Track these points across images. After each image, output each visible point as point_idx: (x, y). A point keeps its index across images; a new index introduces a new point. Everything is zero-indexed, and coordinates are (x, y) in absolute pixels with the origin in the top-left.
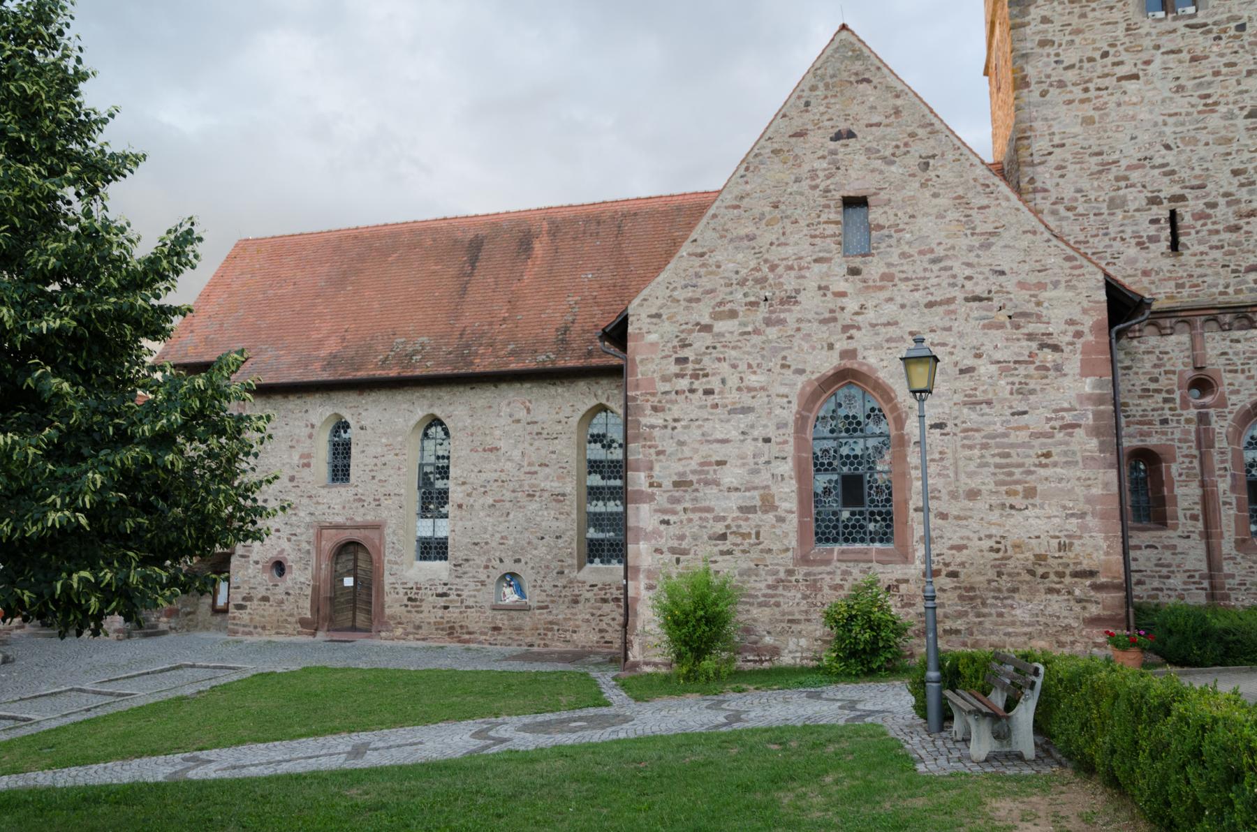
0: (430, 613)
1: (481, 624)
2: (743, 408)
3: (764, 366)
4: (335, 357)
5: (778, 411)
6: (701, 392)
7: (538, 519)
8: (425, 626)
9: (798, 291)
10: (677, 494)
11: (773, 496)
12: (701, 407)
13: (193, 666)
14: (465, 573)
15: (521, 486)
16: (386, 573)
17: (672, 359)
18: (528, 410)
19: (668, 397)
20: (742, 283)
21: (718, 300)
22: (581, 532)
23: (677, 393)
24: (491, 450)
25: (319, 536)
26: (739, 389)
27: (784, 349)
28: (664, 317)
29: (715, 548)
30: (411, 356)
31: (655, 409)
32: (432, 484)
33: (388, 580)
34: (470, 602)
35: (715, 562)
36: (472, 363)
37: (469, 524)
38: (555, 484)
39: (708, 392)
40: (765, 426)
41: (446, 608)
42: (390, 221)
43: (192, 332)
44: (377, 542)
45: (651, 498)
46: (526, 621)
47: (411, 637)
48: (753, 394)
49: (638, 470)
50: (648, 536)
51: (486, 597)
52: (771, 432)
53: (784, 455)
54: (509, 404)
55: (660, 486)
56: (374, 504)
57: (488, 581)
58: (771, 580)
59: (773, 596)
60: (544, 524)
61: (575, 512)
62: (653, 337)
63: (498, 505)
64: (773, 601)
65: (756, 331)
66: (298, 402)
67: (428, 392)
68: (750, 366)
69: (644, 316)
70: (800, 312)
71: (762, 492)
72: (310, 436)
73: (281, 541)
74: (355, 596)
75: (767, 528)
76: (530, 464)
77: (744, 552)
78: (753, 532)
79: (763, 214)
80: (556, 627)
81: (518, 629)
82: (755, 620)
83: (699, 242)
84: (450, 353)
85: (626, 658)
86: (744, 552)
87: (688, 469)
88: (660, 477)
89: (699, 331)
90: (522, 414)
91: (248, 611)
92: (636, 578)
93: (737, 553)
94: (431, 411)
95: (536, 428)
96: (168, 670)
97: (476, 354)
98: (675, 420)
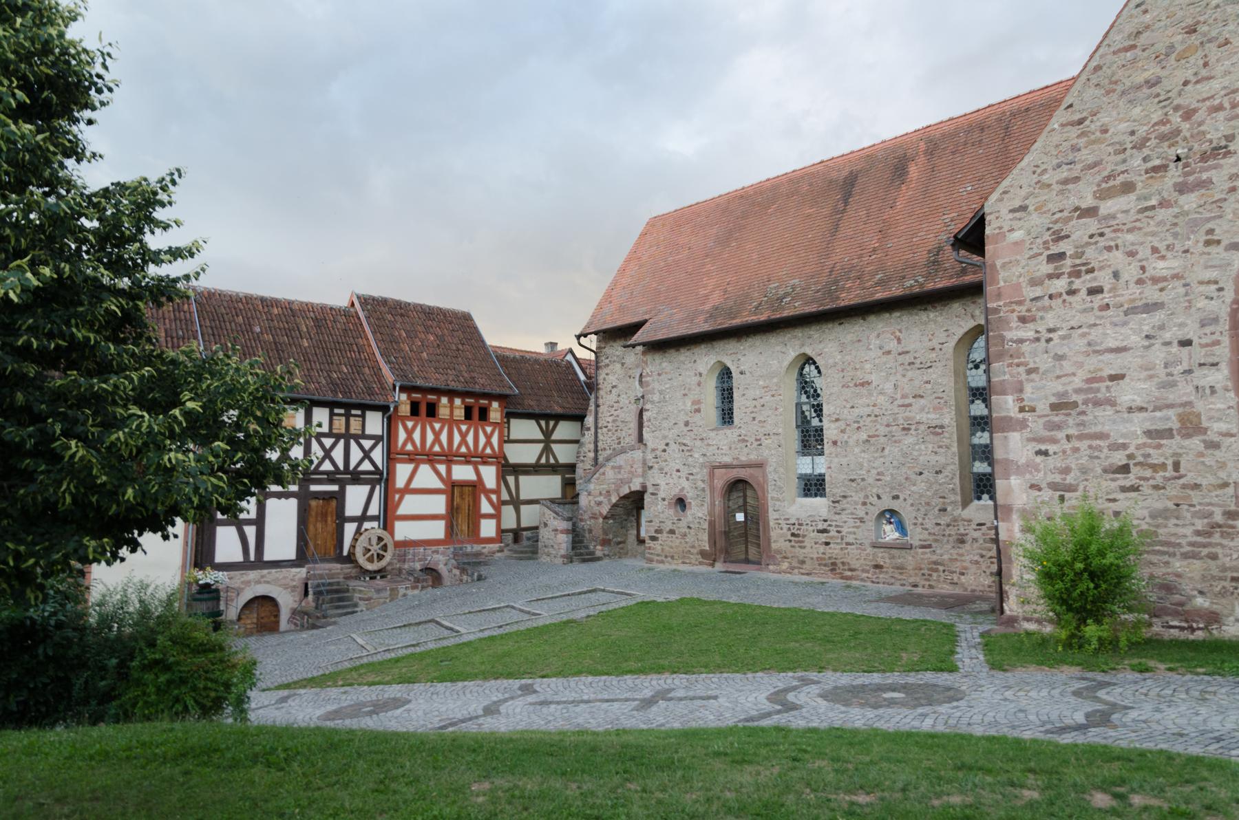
0: (812, 548)
1: (862, 561)
2: (1147, 305)
3: (1178, 247)
4: (717, 309)
5: (1201, 303)
6: (1084, 292)
7: (915, 453)
8: (808, 561)
9: (1230, 138)
10: (1056, 419)
11: (1199, 415)
12: (1085, 311)
13: (603, 591)
14: (843, 510)
15: (894, 420)
16: (770, 509)
17: (1044, 257)
18: (899, 340)
19: (1039, 304)
20: (1139, 146)
21: (1106, 173)
22: (964, 467)
23: (1051, 297)
24: (862, 385)
25: (712, 475)
26: (1140, 282)
27: (1208, 220)
28: (1031, 208)
29: (1111, 484)
30: (781, 299)
31: (1023, 320)
32: (809, 422)
33: (772, 516)
34: (850, 539)
35: (1114, 500)
36: (838, 298)
37: (844, 461)
38: (932, 416)
39: (1095, 291)
40: (1182, 325)
41: (827, 544)
42: (771, 176)
43: (611, 302)
44: (761, 479)
45: (1023, 425)
46: (909, 559)
47: (796, 571)
48: (1161, 285)
49: (1004, 393)
50: (1020, 470)
51: (866, 533)
52: (1191, 332)
53: (1215, 360)
54: (878, 336)
55: (1033, 410)
56: (756, 443)
57: (866, 518)
58: (1200, 524)
59: (1204, 546)
60: (921, 458)
61: (956, 444)
62: (1017, 235)
63: (872, 440)
64: (1205, 551)
65: (1164, 204)
66: (688, 353)
67: (798, 332)
68: (1155, 250)
69: (1004, 212)
70: (1233, 165)
71: (1180, 410)
72: (699, 384)
73: (681, 480)
74: (746, 530)
75: (1191, 457)
76: (904, 397)
77: (1156, 487)
78: (1170, 462)
79: (1172, 47)
80: (941, 568)
81: (900, 568)
82: (1179, 576)
83: (1076, 107)
84: (818, 291)
85: (1002, 611)
86: (1156, 487)
87: (1070, 388)
88: (1032, 400)
89: (1079, 217)
90: (892, 345)
91: (660, 542)
92: (1007, 518)
93: (1146, 490)
94: (802, 351)
95: (908, 358)
96: (585, 593)
97: (843, 289)
98: (1050, 331)
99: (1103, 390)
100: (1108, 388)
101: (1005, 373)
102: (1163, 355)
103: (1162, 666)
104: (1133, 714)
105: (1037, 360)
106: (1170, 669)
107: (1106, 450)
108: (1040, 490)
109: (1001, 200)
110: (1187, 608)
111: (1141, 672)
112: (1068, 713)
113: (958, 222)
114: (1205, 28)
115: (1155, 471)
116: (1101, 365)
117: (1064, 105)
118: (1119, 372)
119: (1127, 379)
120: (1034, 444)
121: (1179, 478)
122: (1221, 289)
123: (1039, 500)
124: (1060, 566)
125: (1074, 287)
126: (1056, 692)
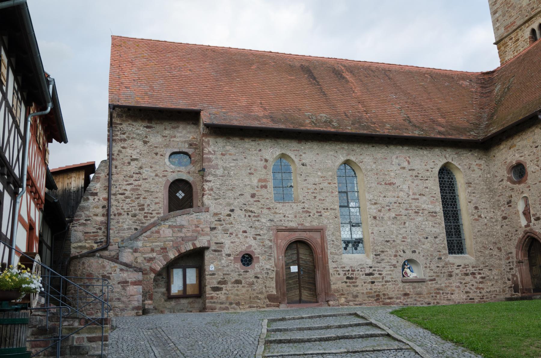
80: (441, 292)
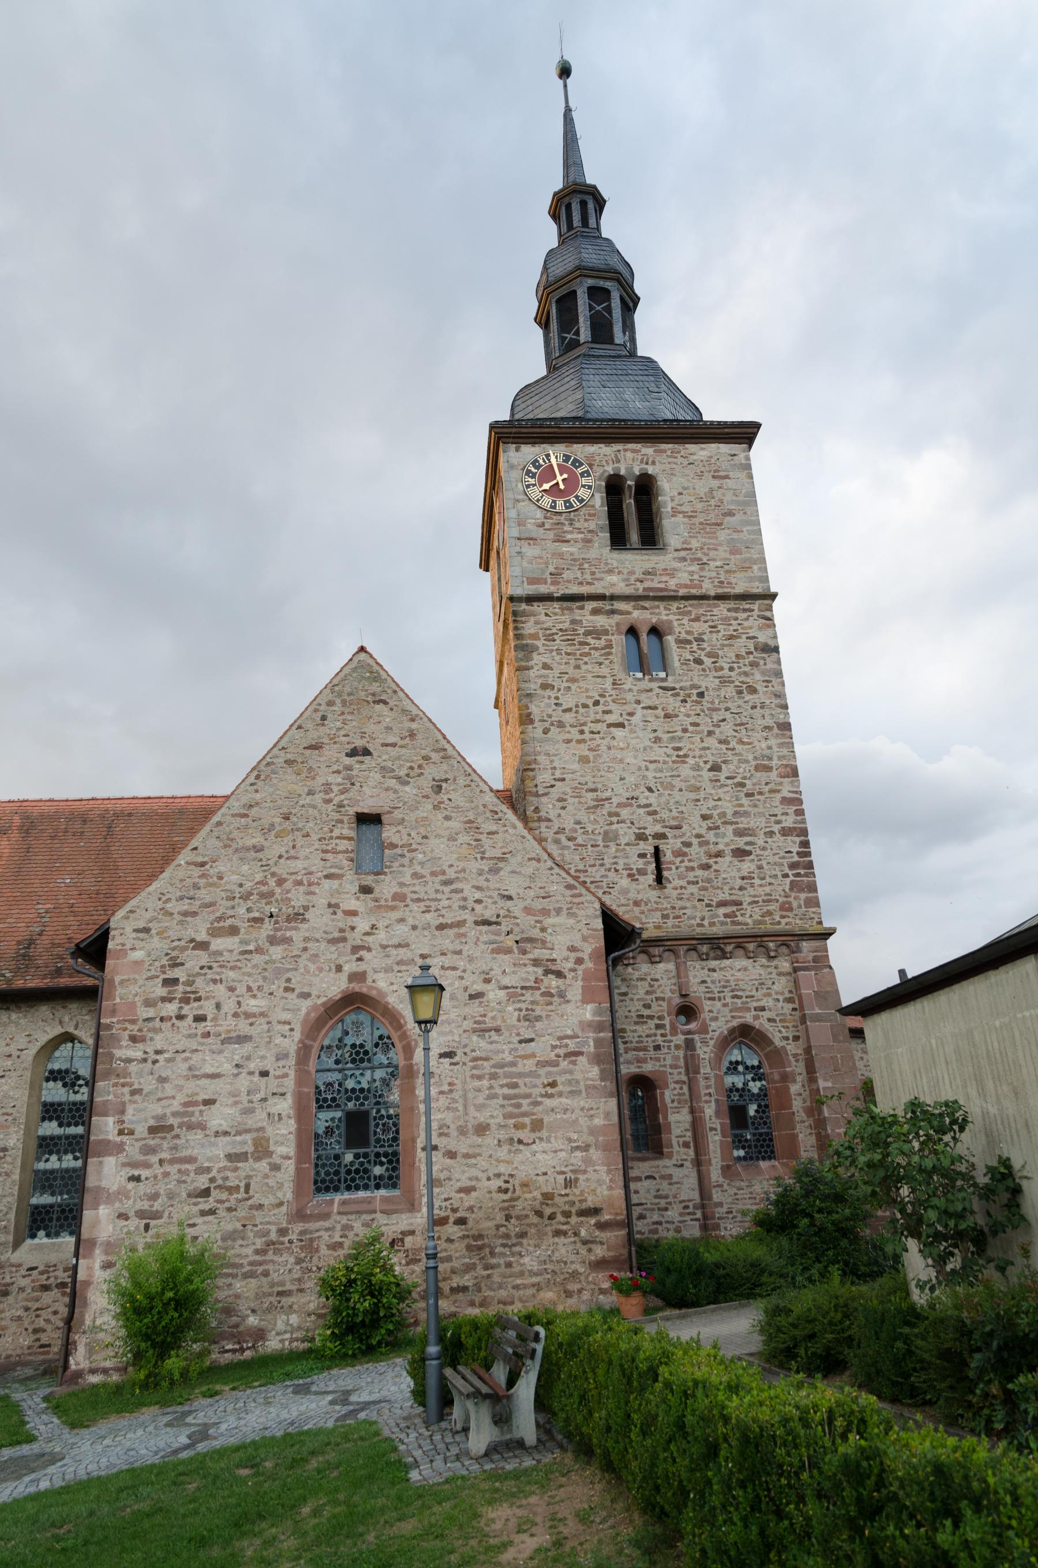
2: (239, 1037)
3: (266, 989)
5: (278, 1040)
6: (190, 1018)
9: (306, 908)
10: (152, 1142)
11: (268, 1140)
12: (189, 1036)
17: (160, 980)
19: (150, 1025)
20: (245, 897)
21: (218, 914)
26: (236, 1015)
28: (153, 932)
31: (133, 1039)
35: (194, 1225)
39: (200, 1019)
40: (263, 1057)
45: (120, 1148)
48: (251, 1020)
52: (269, 1065)
55: (131, 1133)
58: (259, 1243)
61: (18, 1171)
62: (138, 955)
65: (259, 950)
68: (249, 989)
69: (129, 930)
70: (307, 930)
71: (255, 1135)
75: (259, 1179)
77: (230, 1210)
78: (242, 1185)
79: (272, 825)
82: (237, 1296)
83: (200, 851)
86: (230, 1210)
87: (168, 1111)
89: (194, 948)
92: (90, 1255)
93: (222, 1213)
98: (157, 1052)
99: (197, 1114)
100: (201, 1111)
101: (109, 1093)
102: (247, 1083)
103: (227, 1388)
104: (224, 1427)
105: (142, 1080)
106: (233, 1389)
107: (192, 1174)
108: (127, 1219)
109: (127, 918)
110: (241, 1328)
111: (211, 1396)
112: (173, 1440)
113: (84, 933)
114: (295, 819)
115: (231, 1194)
116: (198, 1090)
117: (191, 847)
118: (212, 1097)
119: (217, 1105)
120: (128, 1169)
121: (248, 1199)
122: (292, 1030)
123: (125, 1230)
124: (151, 1298)
125: (183, 1012)
126: (151, 1428)
